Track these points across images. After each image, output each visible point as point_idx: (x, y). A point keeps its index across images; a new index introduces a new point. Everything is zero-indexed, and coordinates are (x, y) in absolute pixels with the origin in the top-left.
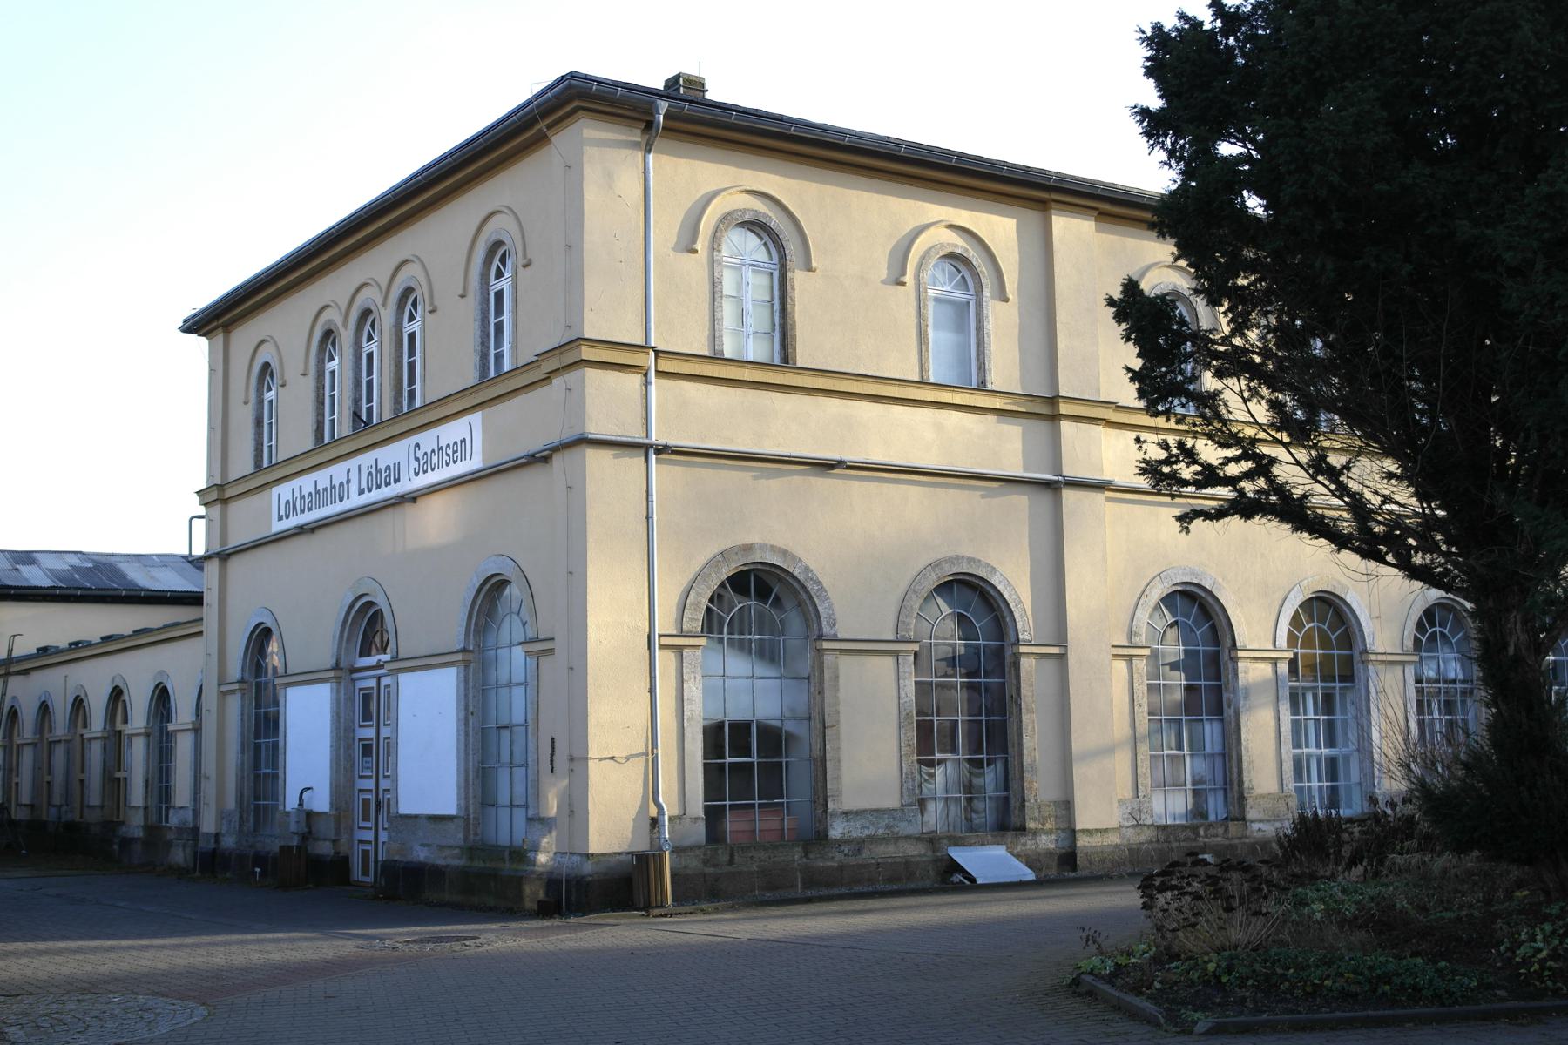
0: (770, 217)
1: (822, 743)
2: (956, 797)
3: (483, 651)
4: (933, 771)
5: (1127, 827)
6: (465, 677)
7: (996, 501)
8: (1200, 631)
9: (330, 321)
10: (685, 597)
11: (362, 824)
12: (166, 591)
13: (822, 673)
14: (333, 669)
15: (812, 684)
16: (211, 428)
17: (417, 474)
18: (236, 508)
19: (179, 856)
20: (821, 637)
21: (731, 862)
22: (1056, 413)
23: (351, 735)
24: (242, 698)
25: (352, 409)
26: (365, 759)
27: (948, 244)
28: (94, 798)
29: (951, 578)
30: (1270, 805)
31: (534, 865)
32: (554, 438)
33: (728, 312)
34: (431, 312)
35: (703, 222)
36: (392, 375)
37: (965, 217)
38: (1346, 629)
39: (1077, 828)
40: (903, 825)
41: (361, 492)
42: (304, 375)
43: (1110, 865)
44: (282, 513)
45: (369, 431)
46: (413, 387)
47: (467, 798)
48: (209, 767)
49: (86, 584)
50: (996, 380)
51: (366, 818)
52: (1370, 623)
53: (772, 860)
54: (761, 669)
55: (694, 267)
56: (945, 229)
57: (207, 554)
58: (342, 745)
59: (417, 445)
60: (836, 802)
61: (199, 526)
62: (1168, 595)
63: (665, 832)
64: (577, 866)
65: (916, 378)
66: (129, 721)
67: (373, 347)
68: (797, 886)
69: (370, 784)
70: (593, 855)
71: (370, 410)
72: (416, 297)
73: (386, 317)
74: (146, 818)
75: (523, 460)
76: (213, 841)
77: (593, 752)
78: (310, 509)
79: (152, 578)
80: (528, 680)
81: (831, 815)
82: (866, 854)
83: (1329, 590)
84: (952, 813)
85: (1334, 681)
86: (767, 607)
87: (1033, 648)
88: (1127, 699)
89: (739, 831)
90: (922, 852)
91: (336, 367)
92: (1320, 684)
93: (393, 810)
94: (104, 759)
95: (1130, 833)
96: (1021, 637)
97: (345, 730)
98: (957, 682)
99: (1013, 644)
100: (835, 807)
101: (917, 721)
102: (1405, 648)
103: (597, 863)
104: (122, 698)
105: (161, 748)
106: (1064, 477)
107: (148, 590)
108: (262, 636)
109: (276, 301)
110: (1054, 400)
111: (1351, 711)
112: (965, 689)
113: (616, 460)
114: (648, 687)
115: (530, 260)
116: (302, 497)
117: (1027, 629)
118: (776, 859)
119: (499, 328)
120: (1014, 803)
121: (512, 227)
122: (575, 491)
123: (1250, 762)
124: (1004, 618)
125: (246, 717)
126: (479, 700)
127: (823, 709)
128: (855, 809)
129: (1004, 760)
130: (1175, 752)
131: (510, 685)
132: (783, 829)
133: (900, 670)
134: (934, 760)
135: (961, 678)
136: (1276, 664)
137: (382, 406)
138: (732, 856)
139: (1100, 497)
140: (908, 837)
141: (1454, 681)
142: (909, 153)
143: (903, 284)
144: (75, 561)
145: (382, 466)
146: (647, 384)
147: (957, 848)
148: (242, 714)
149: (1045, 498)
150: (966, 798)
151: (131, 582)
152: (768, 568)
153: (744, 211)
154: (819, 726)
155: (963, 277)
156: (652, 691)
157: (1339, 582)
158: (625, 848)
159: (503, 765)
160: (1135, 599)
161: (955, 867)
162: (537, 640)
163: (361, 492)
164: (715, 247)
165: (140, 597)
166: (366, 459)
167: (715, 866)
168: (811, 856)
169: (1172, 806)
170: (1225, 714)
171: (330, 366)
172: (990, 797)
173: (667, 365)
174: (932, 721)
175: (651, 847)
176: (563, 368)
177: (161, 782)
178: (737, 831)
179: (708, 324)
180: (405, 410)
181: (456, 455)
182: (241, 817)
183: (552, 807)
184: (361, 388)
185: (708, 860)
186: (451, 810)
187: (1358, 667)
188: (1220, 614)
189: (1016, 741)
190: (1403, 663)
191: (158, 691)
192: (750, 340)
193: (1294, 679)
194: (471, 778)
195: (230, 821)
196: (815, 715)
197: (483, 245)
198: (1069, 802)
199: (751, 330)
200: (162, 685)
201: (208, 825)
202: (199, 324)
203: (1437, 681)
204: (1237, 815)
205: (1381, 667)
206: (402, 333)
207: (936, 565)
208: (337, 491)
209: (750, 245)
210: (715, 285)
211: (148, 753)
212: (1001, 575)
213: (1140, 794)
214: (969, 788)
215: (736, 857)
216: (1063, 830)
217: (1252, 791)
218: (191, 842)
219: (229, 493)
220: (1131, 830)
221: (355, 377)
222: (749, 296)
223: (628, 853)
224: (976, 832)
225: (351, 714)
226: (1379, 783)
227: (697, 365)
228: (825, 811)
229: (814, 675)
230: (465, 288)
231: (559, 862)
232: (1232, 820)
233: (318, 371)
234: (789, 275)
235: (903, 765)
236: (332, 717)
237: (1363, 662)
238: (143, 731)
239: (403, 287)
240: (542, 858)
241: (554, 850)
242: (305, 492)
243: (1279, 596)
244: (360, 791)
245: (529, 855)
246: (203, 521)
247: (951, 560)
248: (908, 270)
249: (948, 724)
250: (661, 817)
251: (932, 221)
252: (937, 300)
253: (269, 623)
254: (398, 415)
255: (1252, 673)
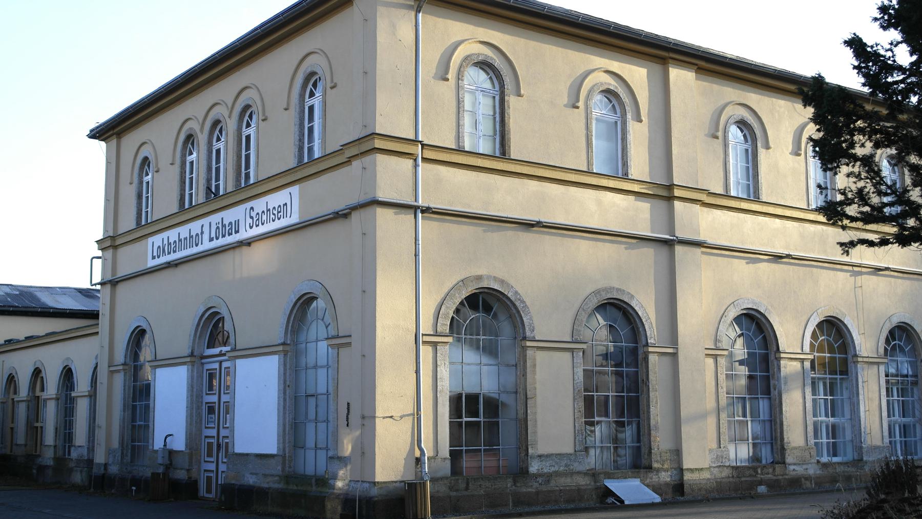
0: (495, 60)
1: (525, 409)
2: (607, 446)
3: (296, 344)
4: (593, 429)
5: (714, 467)
6: (284, 362)
7: (634, 252)
8: (757, 340)
9: (191, 129)
10: (438, 309)
11: (207, 459)
12: (66, 309)
13: (525, 362)
14: (189, 356)
15: (518, 370)
16: (107, 200)
17: (251, 227)
18: (122, 251)
19: (78, 478)
20: (525, 338)
21: (467, 489)
22: (671, 195)
23: (201, 400)
24: (125, 375)
25: (206, 186)
26: (209, 416)
27: (605, 83)
28: (21, 439)
29: (606, 302)
30: (800, 454)
31: (334, 489)
32: (354, 200)
33: (467, 121)
34: (263, 120)
35: (452, 61)
36: (234, 162)
37: (616, 66)
38: (843, 341)
39: (684, 468)
40: (576, 464)
41: (211, 240)
42: (172, 164)
43: (704, 493)
44: (155, 254)
45: (217, 200)
46: (249, 170)
47: (284, 442)
48: (101, 419)
49: (15, 304)
50: (634, 173)
51: (210, 454)
52: (859, 337)
53: (493, 487)
54: (485, 360)
55: (446, 90)
56: (604, 74)
57: (103, 281)
58: (194, 407)
59: (252, 208)
60: (533, 449)
61: (98, 264)
62: (738, 316)
63: (425, 468)
64: (366, 490)
65: (585, 169)
66: (45, 390)
67: (221, 145)
68: (509, 505)
69: (213, 432)
70: (378, 482)
71: (217, 187)
72: (222, 127)
73: (231, 125)
74: (55, 452)
75: (331, 216)
76: (102, 468)
77: (379, 413)
78: (175, 252)
79: (57, 301)
80: (330, 363)
81: (531, 457)
82: (553, 483)
83: (834, 315)
84: (605, 457)
85: (837, 374)
86: (490, 317)
87: (657, 348)
88: (714, 383)
89: (471, 467)
90: (588, 483)
91: (194, 159)
92: (828, 376)
93: (230, 450)
94: (28, 415)
95: (716, 471)
96: (649, 341)
97: (197, 397)
98: (609, 370)
99: (644, 346)
100: (533, 451)
101: (584, 395)
102: (879, 354)
103: (381, 488)
104: (41, 376)
105: (66, 408)
106: (677, 237)
107: (55, 308)
108: (139, 335)
109: (232, 71)
110: (670, 187)
111: (846, 394)
112: (613, 375)
113: (396, 216)
114: (415, 369)
115: (336, 84)
116: (169, 244)
117: (653, 336)
118: (496, 486)
119: (311, 130)
120: (644, 450)
121: (323, 63)
122: (368, 237)
123: (788, 426)
124: (638, 328)
125: (127, 387)
126: (293, 378)
127: (526, 386)
128: (546, 454)
129: (637, 422)
130: (742, 418)
131: (316, 367)
132: (499, 466)
133: (575, 361)
134: (594, 421)
135: (611, 368)
136: (803, 362)
137: (226, 184)
138: (468, 484)
139: (698, 251)
140: (579, 473)
141: (907, 376)
142: (585, 22)
143: (578, 107)
144: (8, 290)
145: (226, 222)
146: (416, 166)
147: (610, 480)
148: (124, 386)
149: (664, 251)
150: (614, 447)
151: (44, 304)
152: (491, 292)
153: (479, 55)
154: (523, 397)
155: (613, 106)
156: (417, 372)
157: (840, 310)
158: (399, 478)
159: (310, 421)
160: (719, 319)
161: (609, 493)
162: (338, 337)
163: (211, 240)
164: (460, 77)
165: (50, 312)
166: (215, 218)
167: (457, 490)
168: (518, 485)
169: (741, 453)
170: (772, 395)
171: (189, 159)
172: (629, 447)
173: (429, 154)
174: (593, 395)
175: (416, 478)
176: (361, 153)
177: (65, 429)
178: (470, 467)
179: (455, 128)
180: (243, 185)
181: (279, 214)
182: (122, 453)
183: (347, 448)
184: (213, 173)
185: (452, 487)
186: (274, 451)
187: (851, 366)
188: (769, 329)
189: (646, 410)
190: (878, 364)
191: (65, 371)
192: (481, 141)
193: (813, 372)
194: (287, 429)
195: (115, 456)
196: (520, 390)
197: (302, 75)
198: (679, 451)
199: (481, 134)
200: (68, 367)
201: (100, 457)
202: (99, 133)
203: (897, 376)
204: (780, 460)
205: (866, 366)
206: (241, 136)
207: (597, 292)
208: (194, 240)
209: (477, 78)
210: (459, 102)
211: (58, 411)
212: (637, 300)
213: (721, 446)
214: (616, 440)
215: (470, 485)
216: (675, 469)
217: (790, 445)
218: (86, 469)
219: (118, 242)
220: (717, 469)
221: (208, 165)
222: (480, 112)
223: (401, 482)
224: (620, 469)
225: (201, 386)
226: (864, 440)
227: (448, 155)
228: (527, 454)
229: (520, 364)
230: (288, 104)
231: (353, 487)
232: (777, 463)
233: (182, 162)
234: (506, 98)
235: (576, 425)
236: (188, 388)
237: (854, 362)
238: (54, 396)
239: (243, 105)
240: (339, 484)
241: (349, 479)
242: (171, 241)
243: (805, 318)
244: (206, 437)
245: (330, 482)
246: (100, 260)
247: (606, 290)
248: (580, 99)
249: (603, 398)
250: (423, 457)
251: (596, 67)
252: (597, 120)
253: (145, 326)
254: (238, 189)
255: (789, 367)
